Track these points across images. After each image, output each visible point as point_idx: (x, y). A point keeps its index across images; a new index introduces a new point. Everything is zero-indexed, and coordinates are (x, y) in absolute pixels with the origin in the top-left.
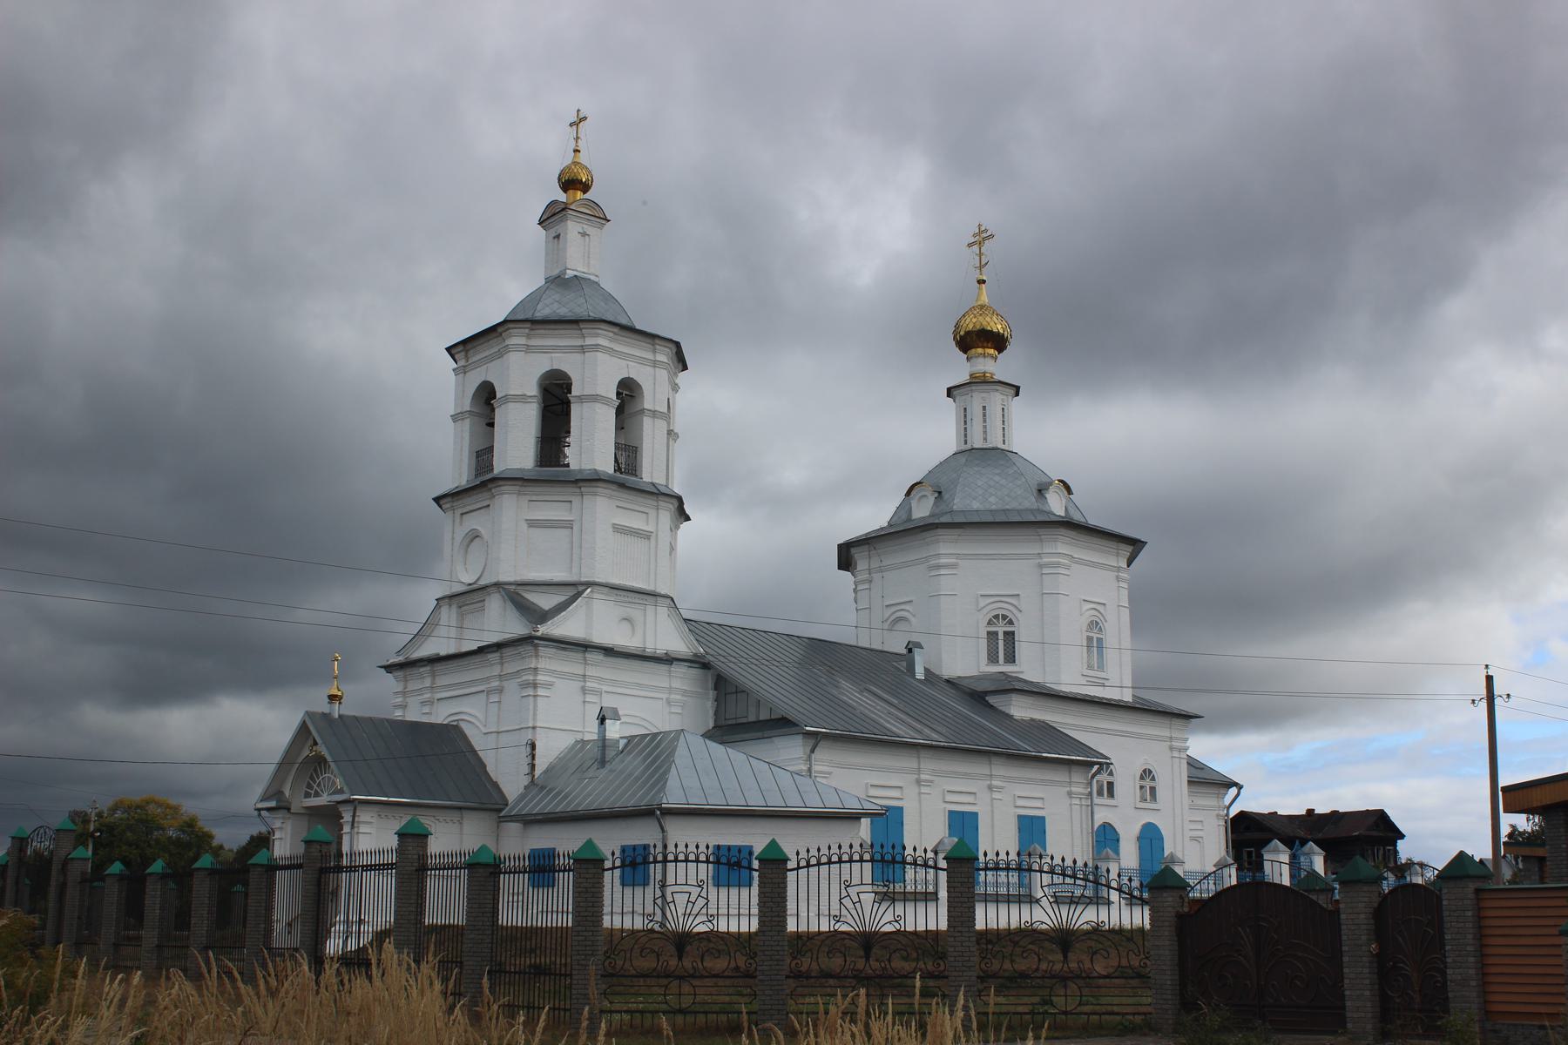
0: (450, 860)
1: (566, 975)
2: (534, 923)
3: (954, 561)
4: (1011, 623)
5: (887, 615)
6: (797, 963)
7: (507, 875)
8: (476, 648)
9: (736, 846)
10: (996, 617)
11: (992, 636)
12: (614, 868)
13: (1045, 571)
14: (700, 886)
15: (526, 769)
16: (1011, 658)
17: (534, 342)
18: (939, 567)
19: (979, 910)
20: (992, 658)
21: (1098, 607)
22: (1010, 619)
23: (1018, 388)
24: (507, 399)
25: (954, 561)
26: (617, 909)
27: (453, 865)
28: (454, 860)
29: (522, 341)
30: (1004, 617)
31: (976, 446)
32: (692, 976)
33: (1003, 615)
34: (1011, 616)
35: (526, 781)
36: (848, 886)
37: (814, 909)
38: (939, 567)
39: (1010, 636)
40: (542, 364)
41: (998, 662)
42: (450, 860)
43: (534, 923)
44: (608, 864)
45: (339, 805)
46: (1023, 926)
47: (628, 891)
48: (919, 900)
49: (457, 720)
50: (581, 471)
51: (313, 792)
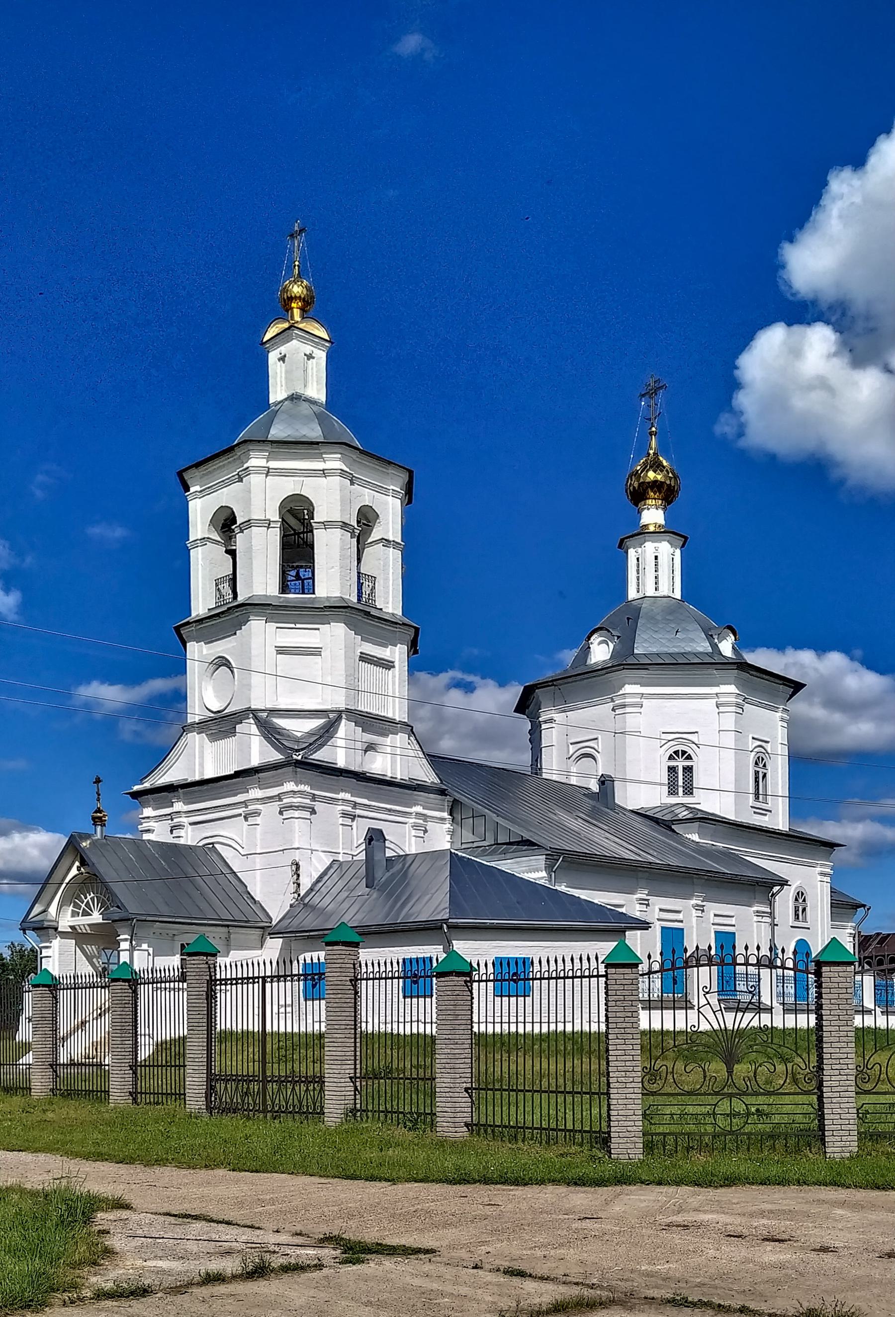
0: (91, 980)
1: (180, 1066)
2: (229, 1026)
3: (639, 700)
4: (689, 758)
5: (571, 752)
6: (865, 1079)
7: (95, 989)
8: (232, 772)
9: (514, 958)
10: (676, 752)
11: (672, 770)
12: (650, 972)
13: (722, 709)
14: (750, 992)
15: (292, 888)
16: (689, 790)
17: (273, 464)
18: (624, 706)
19: (643, 1015)
20: (673, 791)
21: (763, 744)
22: (689, 755)
23: (686, 538)
24: (249, 524)
25: (639, 700)
26: (483, 1019)
27: (94, 985)
28: (88, 980)
29: (262, 462)
30: (684, 752)
31: (647, 595)
32: (745, 1094)
33: (675, 752)
34: (690, 752)
35: (290, 899)
36: (707, 993)
37: (586, 1017)
38: (624, 706)
39: (688, 770)
40: (288, 487)
41: (677, 794)
42: (91, 980)
43: (229, 1026)
44: (643, 968)
45: (116, 925)
46: (689, 1030)
47: (309, 1003)
48: (667, 1008)
49: (213, 843)
50: (328, 598)
51: (81, 911)
